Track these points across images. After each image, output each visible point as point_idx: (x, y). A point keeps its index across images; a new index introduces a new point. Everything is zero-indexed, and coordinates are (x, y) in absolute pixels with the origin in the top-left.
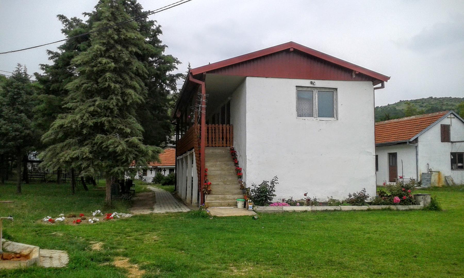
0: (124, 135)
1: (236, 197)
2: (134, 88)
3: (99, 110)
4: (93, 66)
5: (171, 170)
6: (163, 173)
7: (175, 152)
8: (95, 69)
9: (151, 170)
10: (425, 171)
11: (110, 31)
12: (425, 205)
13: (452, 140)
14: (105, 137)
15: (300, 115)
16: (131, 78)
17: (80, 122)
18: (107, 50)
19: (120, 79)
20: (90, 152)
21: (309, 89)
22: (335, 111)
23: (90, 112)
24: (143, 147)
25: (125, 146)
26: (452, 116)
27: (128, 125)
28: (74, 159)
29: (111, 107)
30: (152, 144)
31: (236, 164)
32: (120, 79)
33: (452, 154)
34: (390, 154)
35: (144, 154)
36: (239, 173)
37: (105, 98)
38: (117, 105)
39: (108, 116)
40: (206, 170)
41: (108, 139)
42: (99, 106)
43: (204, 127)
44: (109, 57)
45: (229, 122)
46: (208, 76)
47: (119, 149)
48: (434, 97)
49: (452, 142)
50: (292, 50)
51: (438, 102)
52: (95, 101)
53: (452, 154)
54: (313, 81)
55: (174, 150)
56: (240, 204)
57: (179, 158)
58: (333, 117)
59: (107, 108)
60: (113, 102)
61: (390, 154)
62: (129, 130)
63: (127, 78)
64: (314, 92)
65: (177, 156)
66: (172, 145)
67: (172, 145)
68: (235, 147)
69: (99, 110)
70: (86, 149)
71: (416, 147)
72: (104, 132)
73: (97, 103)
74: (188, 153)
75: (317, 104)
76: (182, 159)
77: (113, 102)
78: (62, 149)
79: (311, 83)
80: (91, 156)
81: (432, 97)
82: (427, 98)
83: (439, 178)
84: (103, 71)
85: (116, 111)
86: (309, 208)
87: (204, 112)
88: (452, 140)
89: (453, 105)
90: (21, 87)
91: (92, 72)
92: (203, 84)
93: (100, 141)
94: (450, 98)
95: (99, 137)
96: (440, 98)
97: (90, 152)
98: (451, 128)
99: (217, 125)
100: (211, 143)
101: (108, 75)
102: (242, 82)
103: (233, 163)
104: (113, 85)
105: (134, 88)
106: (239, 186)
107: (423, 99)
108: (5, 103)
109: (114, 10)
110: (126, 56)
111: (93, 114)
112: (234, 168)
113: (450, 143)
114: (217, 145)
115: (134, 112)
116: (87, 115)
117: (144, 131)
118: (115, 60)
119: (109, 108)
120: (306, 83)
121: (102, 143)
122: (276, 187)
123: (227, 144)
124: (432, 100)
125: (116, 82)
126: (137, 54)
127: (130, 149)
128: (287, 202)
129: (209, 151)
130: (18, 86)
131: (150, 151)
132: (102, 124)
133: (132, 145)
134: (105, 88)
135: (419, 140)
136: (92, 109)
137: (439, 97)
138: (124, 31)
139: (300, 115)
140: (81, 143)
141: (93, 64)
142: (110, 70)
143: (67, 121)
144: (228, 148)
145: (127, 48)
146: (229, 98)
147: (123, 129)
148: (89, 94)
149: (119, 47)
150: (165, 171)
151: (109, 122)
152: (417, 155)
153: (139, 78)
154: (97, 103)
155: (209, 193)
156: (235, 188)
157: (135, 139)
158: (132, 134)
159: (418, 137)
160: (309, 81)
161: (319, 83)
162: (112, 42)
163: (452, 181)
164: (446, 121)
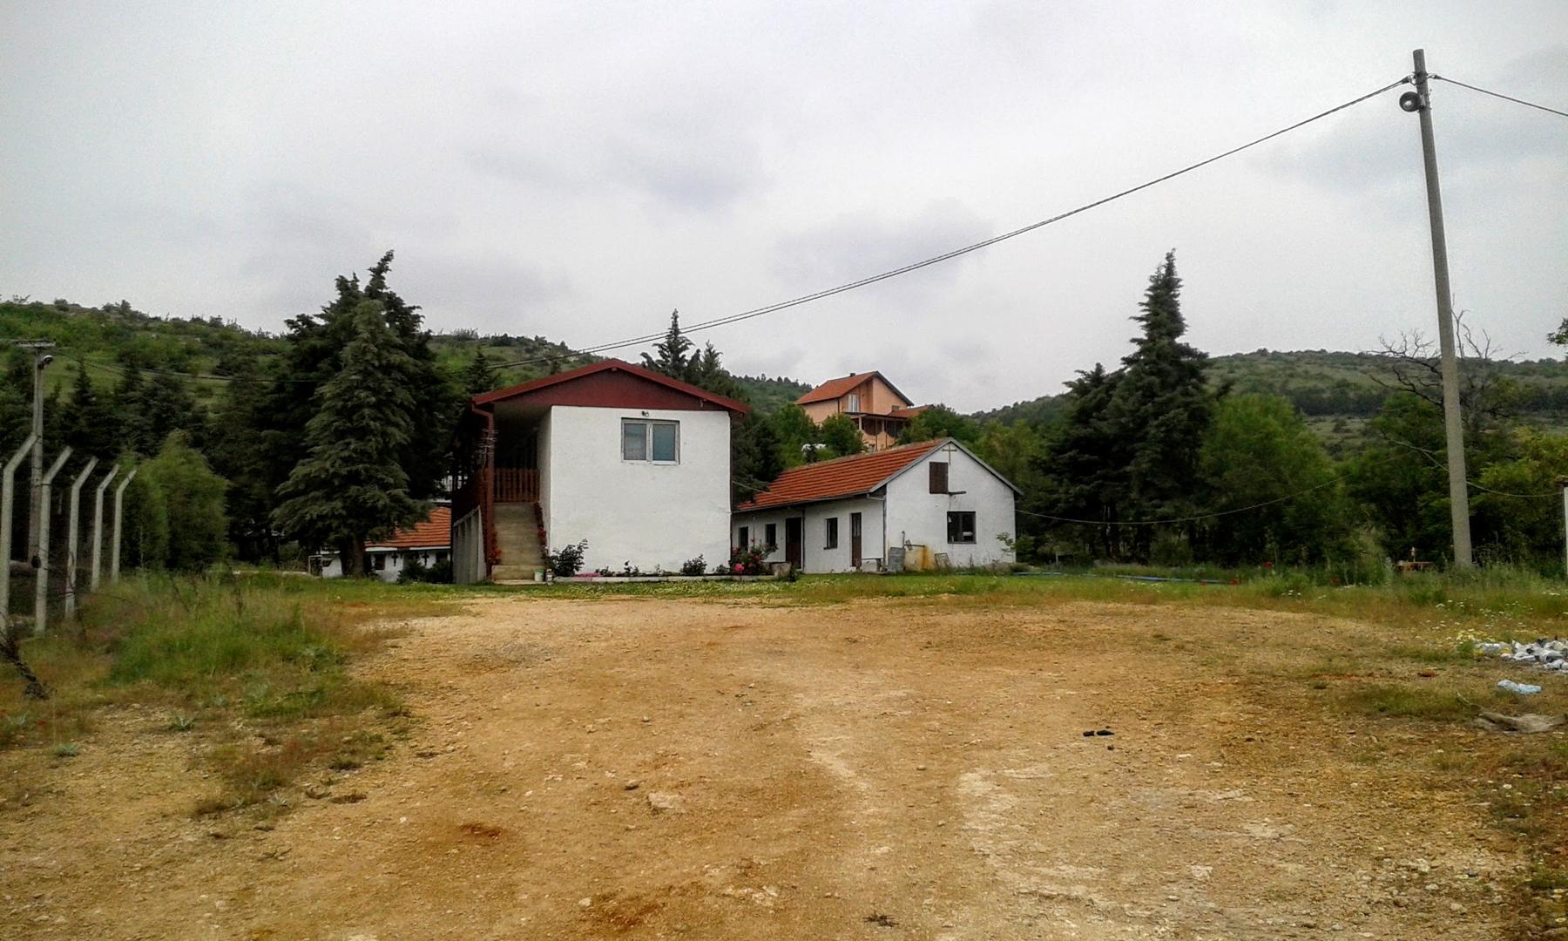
0: (385, 487)
1: (534, 568)
2: (397, 425)
3: (355, 456)
4: (347, 401)
5: (440, 555)
6: (422, 561)
7: (449, 516)
8: (350, 403)
9: (395, 557)
10: (899, 545)
11: (369, 357)
12: (779, 575)
13: (950, 490)
14: (362, 489)
15: (627, 455)
16: (393, 412)
17: (332, 470)
18: (364, 380)
19: (380, 415)
20: (343, 508)
21: (641, 422)
22: (677, 452)
23: (341, 458)
24: (410, 501)
25: (388, 501)
26: (952, 447)
27: (391, 474)
28: (321, 517)
29: (370, 450)
30: (420, 499)
31: (541, 525)
32: (380, 415)
33: (949, 514)
34: (853, 515)
35: (410, 510)
36: (542, 538)
37: (361, 439)
38: (377, 448)
39: (365, 463)
40: (495, 535)
41: (366, 492)
42: (355, 451)
43: (490, 471)
44: (368, 388)
45: (535, 467)
46: (496, 404)
47: (381, 503)
48: (1270, 351)
49: (951, 494)
50: (614, 369)
51: (1281, 367)
52: (349, 443)
53: (949, 514)
54: (645, 411)
55: (449, 511)
56: (538, 577)
57: (458, 522)
58: (674, 460)
59: (363, 452)
60: (372, 444)
61: (853, 515)
62: (391, 481)
63: (388, 412)
64: (648, 426)
65: (453, 520)
66: (443, 501)
67: (443, 501)
68: (541, 502)
69: (355, 456)
70: (338, 504)
71: (884, 502)
72: (360, 483)
73: (352, 447)
74: (472, 512)
75: (651, 442)
76: (463, 524)
77: (372, 444)
78: (304, 504)
79: (643, 413)
80: (344, 513)
81: (1265, 350)
82: (1251, 354)
83: (925, 558)
84: (359, 407)
85: (375, 457)
86: (626, 579)
87: (491, 454)
88: (950, 490)
89: (1322, 377)
90: (173, 398)
91: (344, 407)
92: (490, 416)
93: (354, 495)
94: (1319, 352)
95: (353, 490)
96: (1290, 354)
97: (343, 508)
98: (950, 469)
99: (514, 469)
100: (502, 495)
101: (366, 411)
102: (550, 409)
103: (535, 525)
104: (372, 423)
105: (397, 425)
106: (540, 554)
107: (1238, 357)
108: (149, 428)
109: (373, 328)
110: (388, 385)
111: (346, 460)
112: (537, 531)
113: (947, 496)
114: (504, 499)
115: (396, 456)
116: (339, 462)
117: (408, 479)
118: (375, 392)
119: (366, 452)
120: (635, 413)
121: (357, 496)
122: (585, 554)
123: (501, 496)
124: (1264, 359)
125: (374, 419)
126: (402, 382)
127: (393, 504)
128: (602, 573)
129: (501, 508)
130: (168, 395)
131: (419, 507)
132: (358, 472)
133: (395, 499)
134: (363, 427)
135: (888, 490)
136: (346, 454)
137: (1287, 351)
138: (385, 353)
139: (627, 455)
140: (329, 498)
141: (346, 397)
142: (369, 406)
143: (313, 470)
144: (532, 503)
145: (389, 374)
146: (535, 429)
147: (383, 479)
148: (340, 434)
149: (380, 375)
150: (426, 557)
151: (366, 470)
152: (884, 515)
153: (403, 411)
154: (352, 447)
155: (498, 562)
156: (533, 557)
157: (399, 492)
158: (396, 486)
159: (885, 486)
160: (640, 411)
161: (654, 414)
162: (370, 368)
163: (946, 561)
164: (940, 457)
